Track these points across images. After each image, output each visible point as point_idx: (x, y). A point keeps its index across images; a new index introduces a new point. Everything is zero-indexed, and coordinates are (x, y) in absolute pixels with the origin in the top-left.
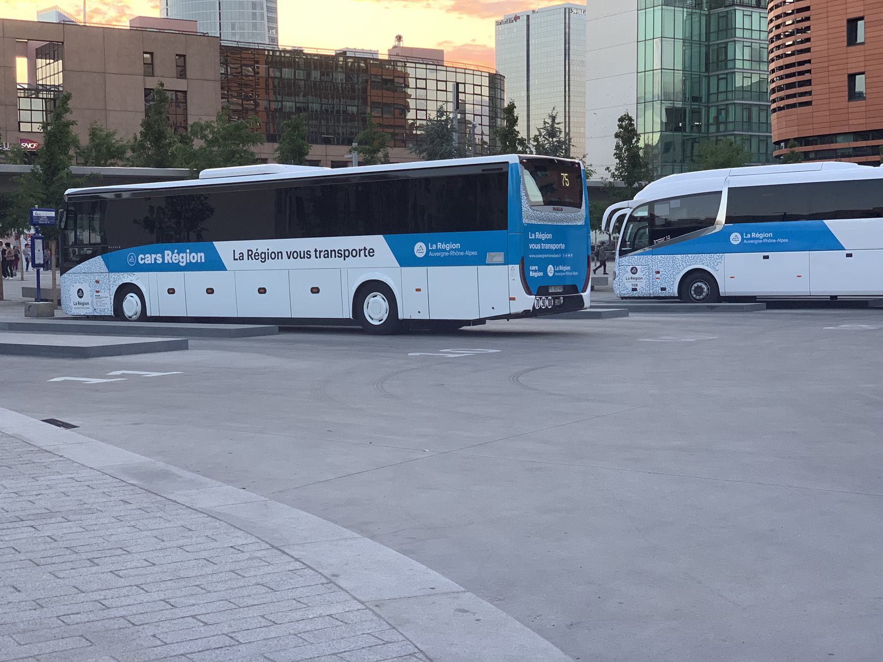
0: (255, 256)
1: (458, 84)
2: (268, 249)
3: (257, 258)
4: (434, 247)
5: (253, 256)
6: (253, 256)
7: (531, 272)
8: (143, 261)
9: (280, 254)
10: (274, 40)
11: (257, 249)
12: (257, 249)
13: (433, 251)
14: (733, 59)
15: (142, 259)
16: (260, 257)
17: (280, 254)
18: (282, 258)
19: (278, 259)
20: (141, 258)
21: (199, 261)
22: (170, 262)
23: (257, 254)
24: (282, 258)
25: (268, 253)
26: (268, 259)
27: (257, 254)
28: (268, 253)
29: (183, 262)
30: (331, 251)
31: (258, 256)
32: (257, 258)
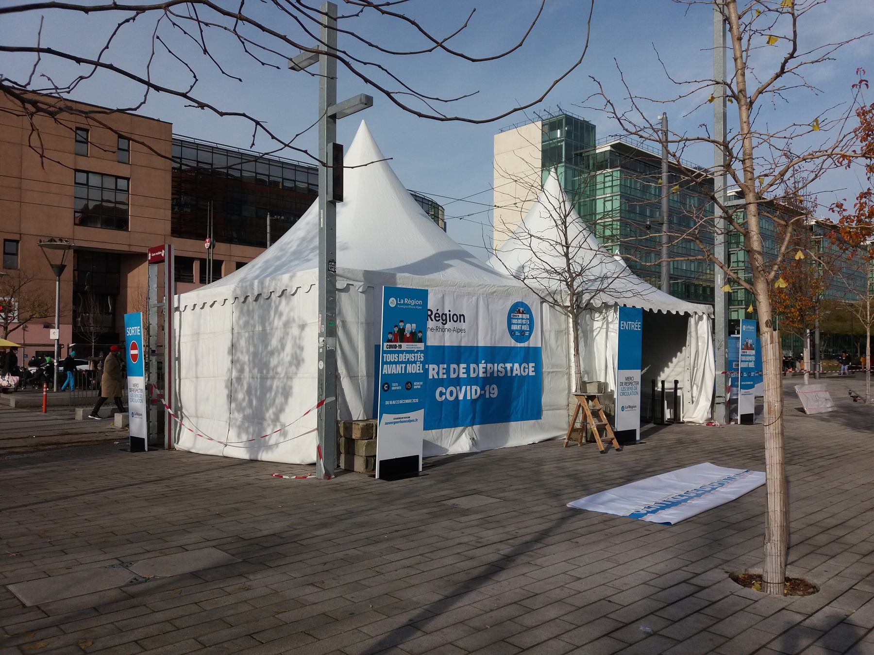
0: (435, 317)
1: (128, 179)
2: (450, 311)
3: (437, 319)
4: (402, 302)
5: (433, 317)
6: (433, 317)
7: (445, 366)
8: (444, 397)
9: (462, 317)
10: (395, 282)
11: (438, 310)
12: (438, 310)
13: (400, 304)
14: (114, 180)
15: (441, 394)
16: (440, 318)
17: (462, 317)
18: (464, 322)
19: (460, 322)
20: (441, 392)
21: (400, 372)
22: (436, 377)
23: (437, 315)
24: (464, 322)
25: (450, 314)
26: (450, 321)
27: (437, 315)
28: (450, 314)
29: (493, 394)
30: (460, 316)
31: (439, 317)
32: (437, 319)
